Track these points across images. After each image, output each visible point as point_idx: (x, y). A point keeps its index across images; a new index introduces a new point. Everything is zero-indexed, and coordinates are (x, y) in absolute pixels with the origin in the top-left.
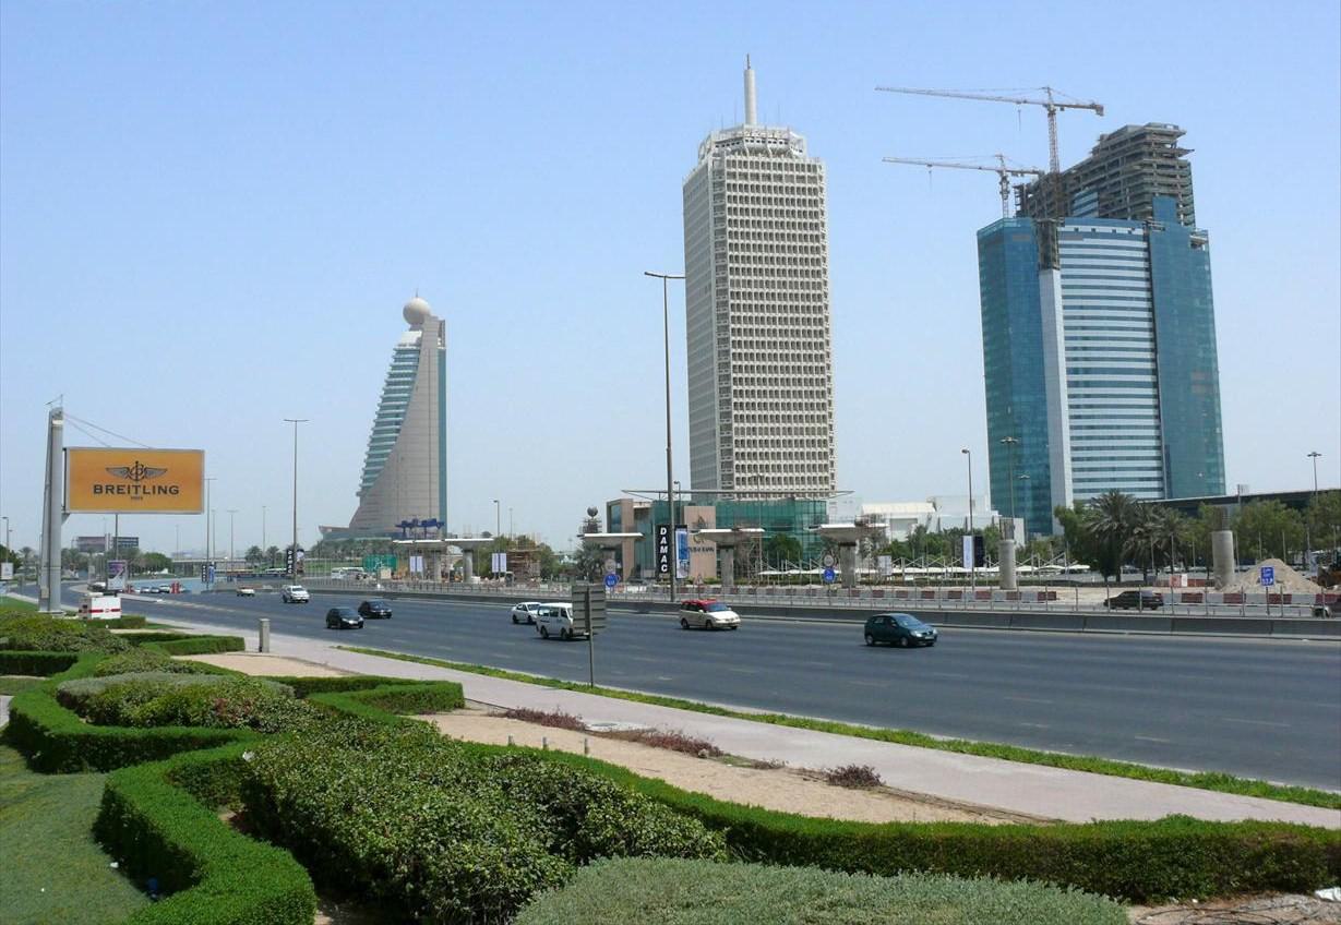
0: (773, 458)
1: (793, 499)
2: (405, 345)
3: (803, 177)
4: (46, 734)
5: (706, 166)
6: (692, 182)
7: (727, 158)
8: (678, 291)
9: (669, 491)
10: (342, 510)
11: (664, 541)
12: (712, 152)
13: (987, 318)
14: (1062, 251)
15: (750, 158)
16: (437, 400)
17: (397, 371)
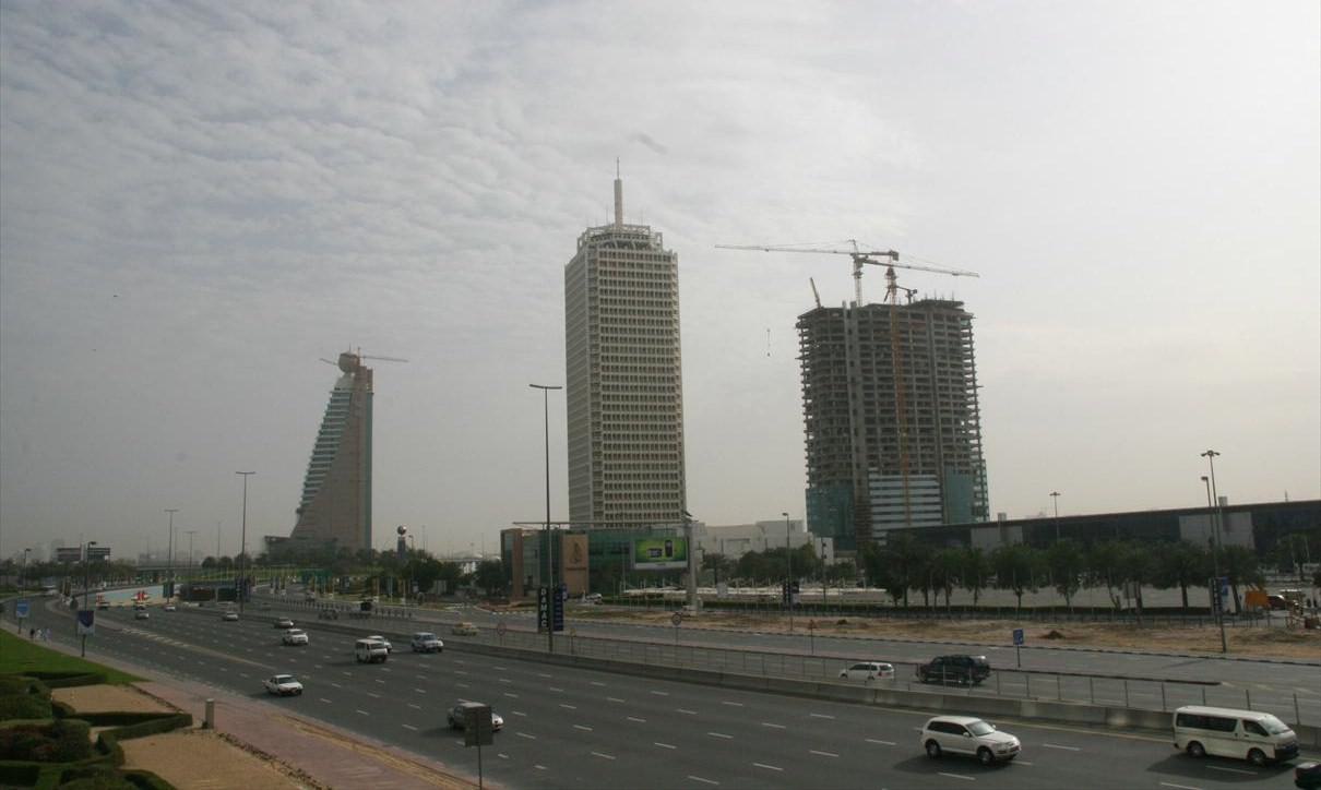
1: (650, 527)
4: (106, 558)
8: (560, 400)
9: (548, 523)
10: (284, 524)
11: (544, 600)
15: (617, 250)
17: (322, 450)
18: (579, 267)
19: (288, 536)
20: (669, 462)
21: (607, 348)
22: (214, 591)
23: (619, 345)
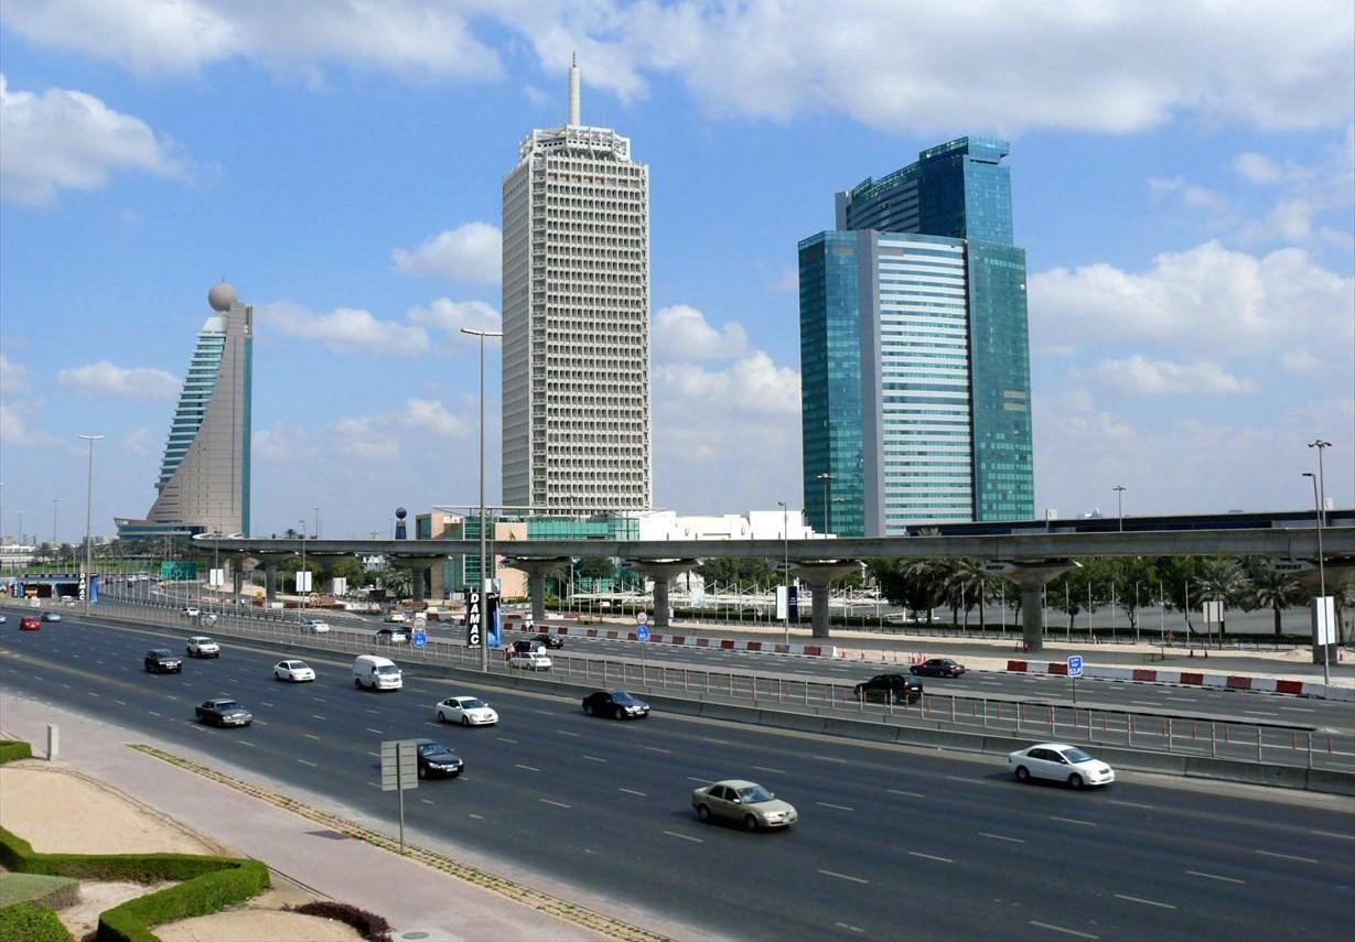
0: (586, 428)
2: (210, 332)
3: (626, 181)
5: (527, 165)
6: (511, 180)
7: (548, 158)
12: (533, 152)
13: (805, 311)
14: (882, 266)
16: (242, 390)
18: (520, 191)
19: (145, 519)
20: (632, 433)
21: (556, 285)
22: (50, 587)
23: (572, 282)
